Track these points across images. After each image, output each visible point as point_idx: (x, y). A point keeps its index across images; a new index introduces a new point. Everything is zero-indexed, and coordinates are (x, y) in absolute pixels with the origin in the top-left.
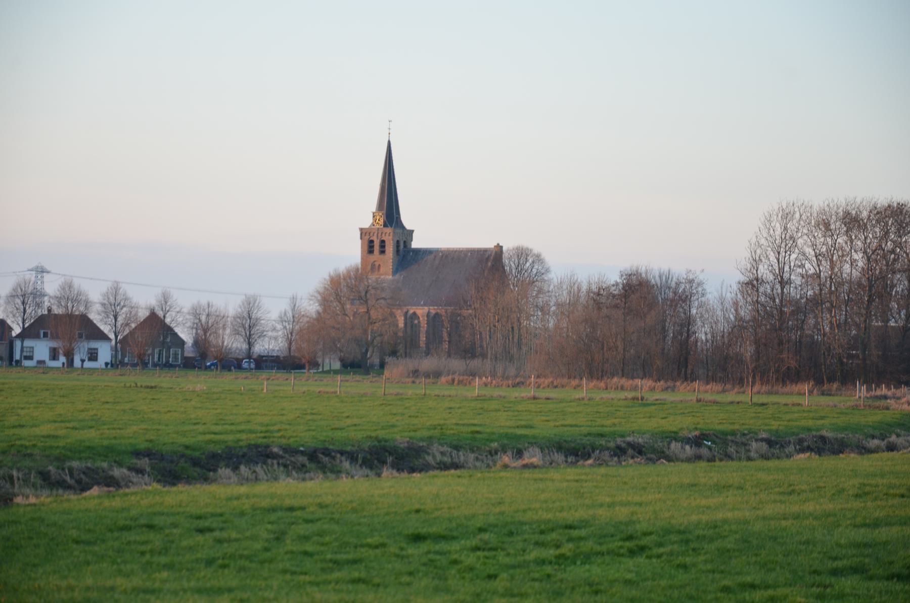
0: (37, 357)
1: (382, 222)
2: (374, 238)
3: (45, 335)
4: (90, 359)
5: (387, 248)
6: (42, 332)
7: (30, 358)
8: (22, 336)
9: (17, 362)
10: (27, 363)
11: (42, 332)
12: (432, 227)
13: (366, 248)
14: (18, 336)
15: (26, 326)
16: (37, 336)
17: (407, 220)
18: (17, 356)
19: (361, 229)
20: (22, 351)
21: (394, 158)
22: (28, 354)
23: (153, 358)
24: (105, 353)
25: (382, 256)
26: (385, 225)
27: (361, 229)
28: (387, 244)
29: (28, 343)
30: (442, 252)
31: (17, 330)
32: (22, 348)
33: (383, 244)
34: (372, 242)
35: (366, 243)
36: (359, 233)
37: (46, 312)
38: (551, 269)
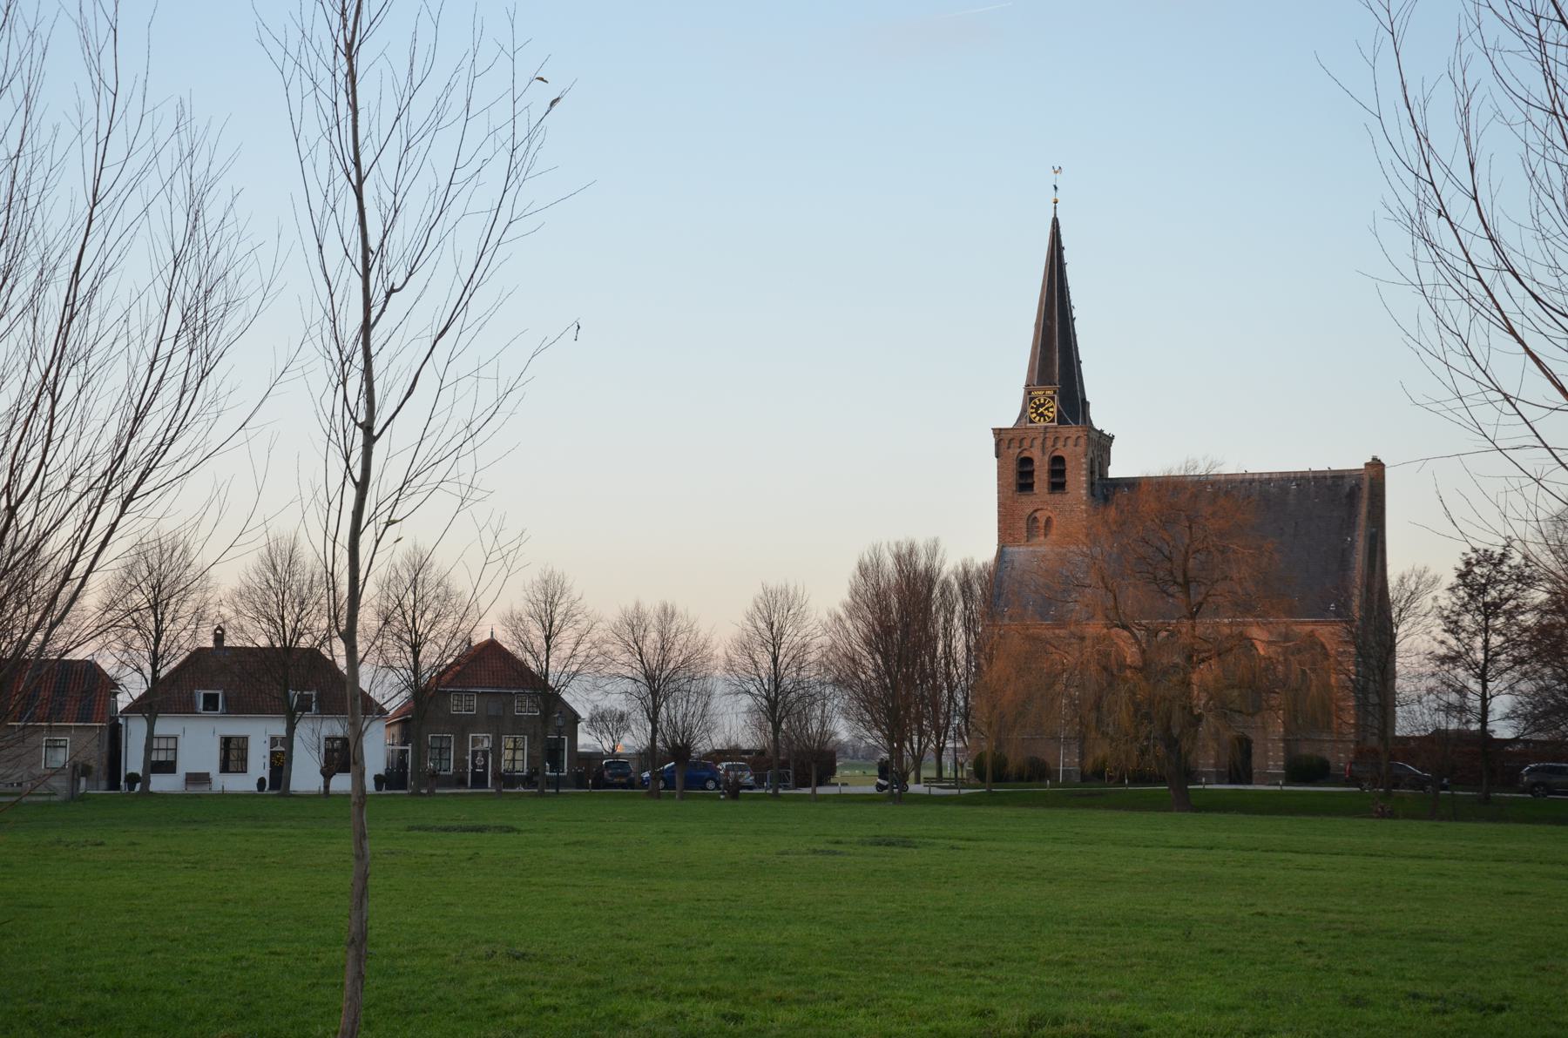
0: (186, 765)
1: (1053, 412)
2: (1036, 453)
3: (211, 702)
4: (225, 768)
5: (1069, 476)
6: (200, 695)
7: (169, 767)
8: (147, 706)
9: (133, 779)
10: (159, 783)
11: (200, 695)
12: (1152, 429)
13: (1012, 478)
14: (136, 707)
15: (163, 673)
16: (185, 708)
17: (1099, 418)
18: (134, 762)
19: (998, 433)
20: (149, 749)
21: (1068, 268)
22: (162, 757)
23: (497, 761)
24: (377, 749)
25: (1057, 497)
26: (1062, 420)
27: (998, 433)
28: (1070, 466)
29: (164, 726)
30: (1213, 484)
31: (133, 687)
32: (150, 736)
33: (1058, 467)
34: (1025, 462)
35: (1013, 466)
36: (990, 442)
37: (210, 644)
38: (678, 610)
